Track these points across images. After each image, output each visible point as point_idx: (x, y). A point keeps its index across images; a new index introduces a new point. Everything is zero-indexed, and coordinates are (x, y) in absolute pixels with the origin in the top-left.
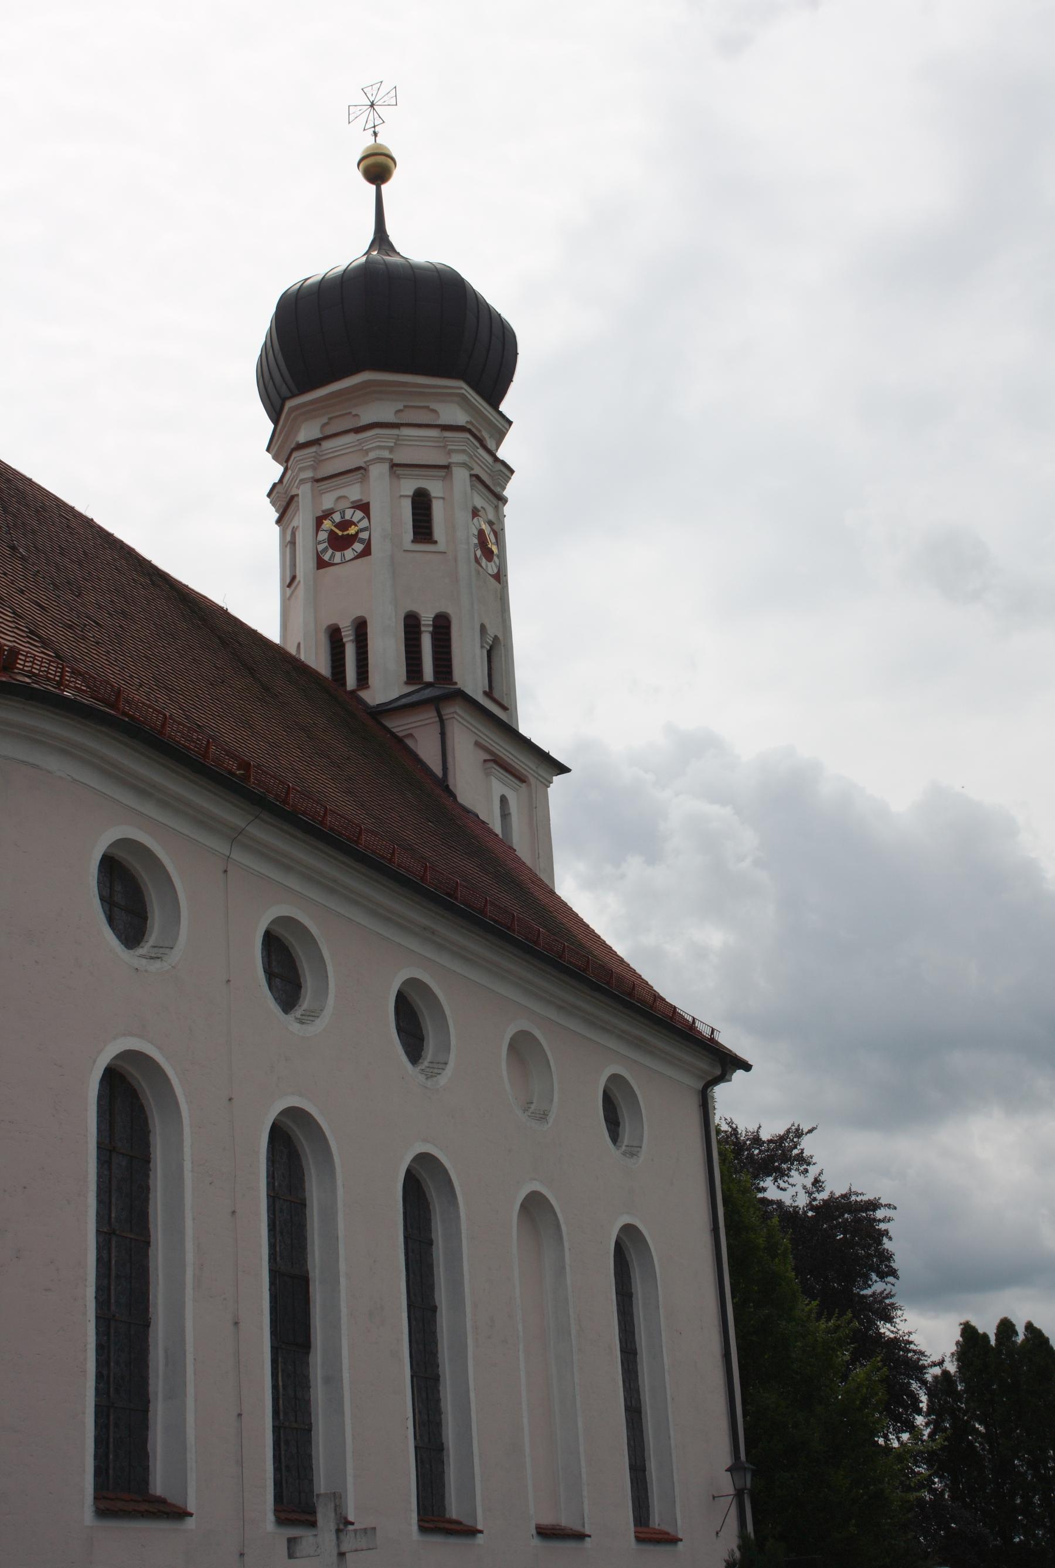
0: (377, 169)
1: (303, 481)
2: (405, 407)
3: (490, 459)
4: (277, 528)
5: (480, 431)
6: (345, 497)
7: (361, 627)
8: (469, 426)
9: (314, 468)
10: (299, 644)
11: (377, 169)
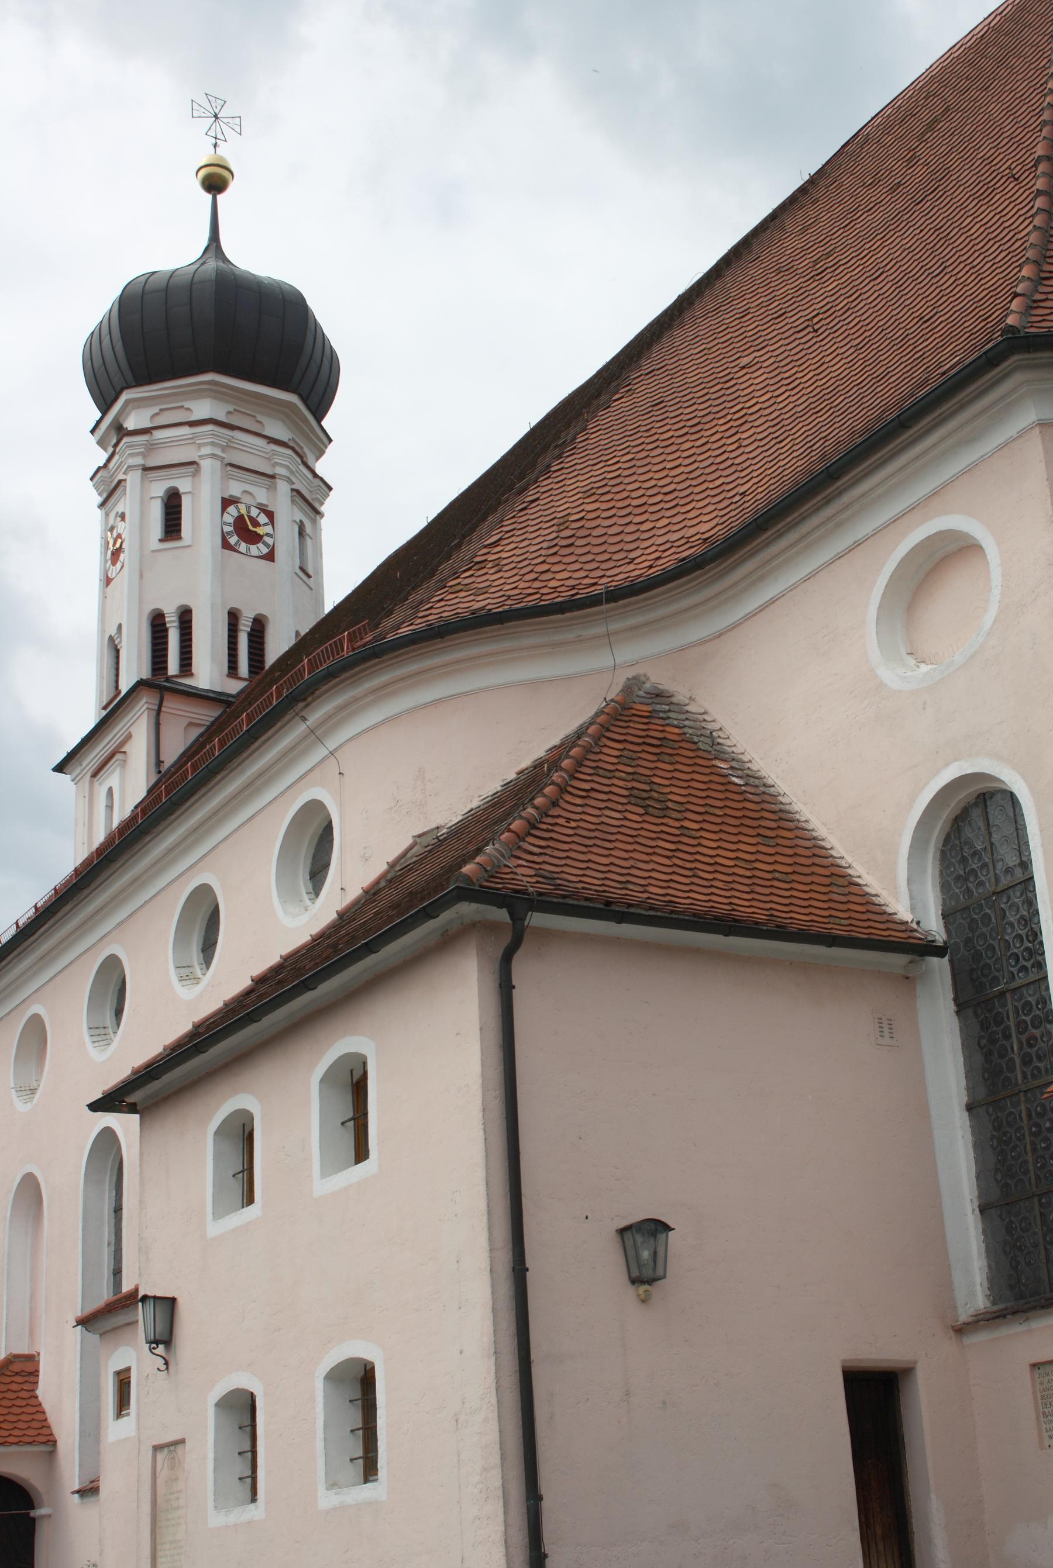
0: (215, 183)
1: (131, 468)
2: (161, 410)
3: (310, 475)
4: (99, 514)
5: (302, 448)
6: (251, 494)
7: (185, 617)
8: (291, 444)
9: (144, 455)
10: (120, 626)
11: (215, 183)
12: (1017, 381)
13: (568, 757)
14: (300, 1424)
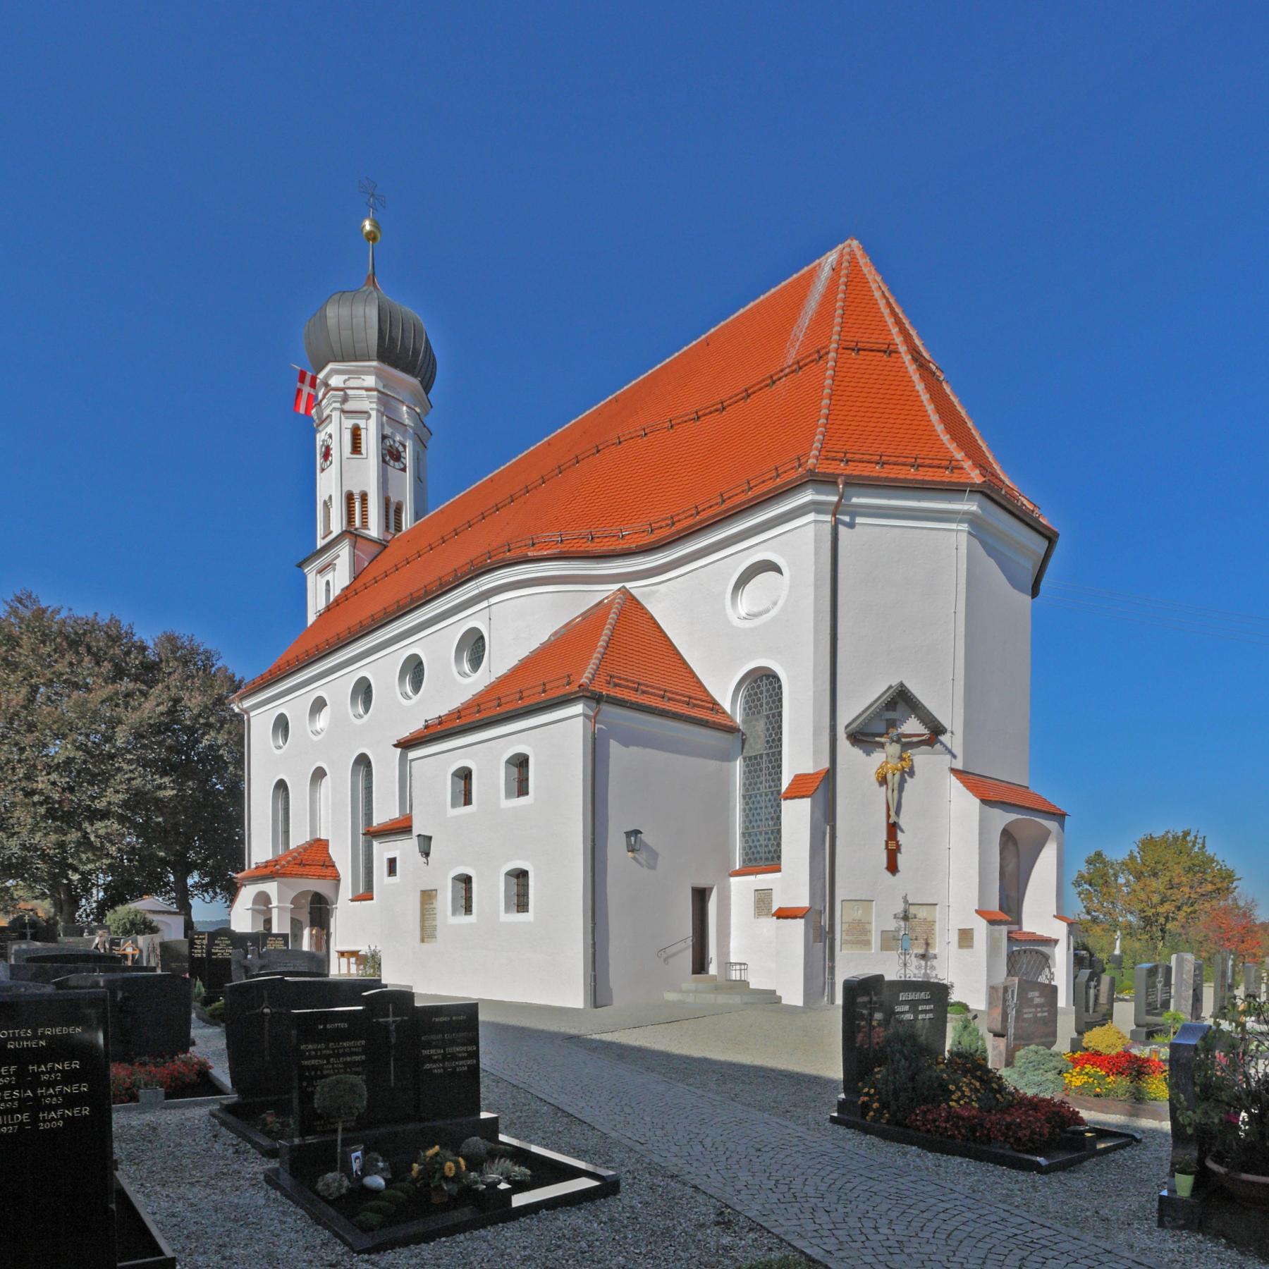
7: (364, 497)
12: (810, 485)
13: (875, 1111)
14: (491, 891)
